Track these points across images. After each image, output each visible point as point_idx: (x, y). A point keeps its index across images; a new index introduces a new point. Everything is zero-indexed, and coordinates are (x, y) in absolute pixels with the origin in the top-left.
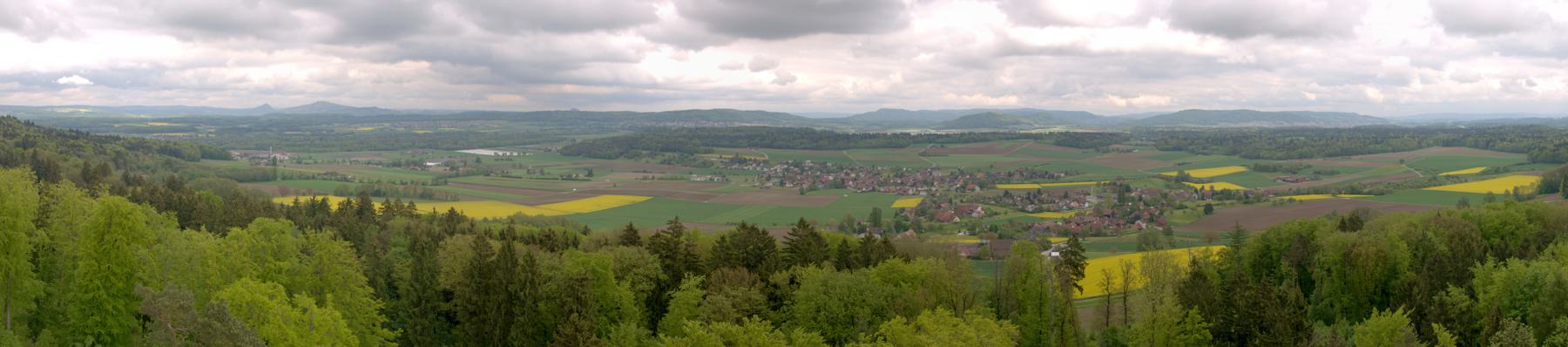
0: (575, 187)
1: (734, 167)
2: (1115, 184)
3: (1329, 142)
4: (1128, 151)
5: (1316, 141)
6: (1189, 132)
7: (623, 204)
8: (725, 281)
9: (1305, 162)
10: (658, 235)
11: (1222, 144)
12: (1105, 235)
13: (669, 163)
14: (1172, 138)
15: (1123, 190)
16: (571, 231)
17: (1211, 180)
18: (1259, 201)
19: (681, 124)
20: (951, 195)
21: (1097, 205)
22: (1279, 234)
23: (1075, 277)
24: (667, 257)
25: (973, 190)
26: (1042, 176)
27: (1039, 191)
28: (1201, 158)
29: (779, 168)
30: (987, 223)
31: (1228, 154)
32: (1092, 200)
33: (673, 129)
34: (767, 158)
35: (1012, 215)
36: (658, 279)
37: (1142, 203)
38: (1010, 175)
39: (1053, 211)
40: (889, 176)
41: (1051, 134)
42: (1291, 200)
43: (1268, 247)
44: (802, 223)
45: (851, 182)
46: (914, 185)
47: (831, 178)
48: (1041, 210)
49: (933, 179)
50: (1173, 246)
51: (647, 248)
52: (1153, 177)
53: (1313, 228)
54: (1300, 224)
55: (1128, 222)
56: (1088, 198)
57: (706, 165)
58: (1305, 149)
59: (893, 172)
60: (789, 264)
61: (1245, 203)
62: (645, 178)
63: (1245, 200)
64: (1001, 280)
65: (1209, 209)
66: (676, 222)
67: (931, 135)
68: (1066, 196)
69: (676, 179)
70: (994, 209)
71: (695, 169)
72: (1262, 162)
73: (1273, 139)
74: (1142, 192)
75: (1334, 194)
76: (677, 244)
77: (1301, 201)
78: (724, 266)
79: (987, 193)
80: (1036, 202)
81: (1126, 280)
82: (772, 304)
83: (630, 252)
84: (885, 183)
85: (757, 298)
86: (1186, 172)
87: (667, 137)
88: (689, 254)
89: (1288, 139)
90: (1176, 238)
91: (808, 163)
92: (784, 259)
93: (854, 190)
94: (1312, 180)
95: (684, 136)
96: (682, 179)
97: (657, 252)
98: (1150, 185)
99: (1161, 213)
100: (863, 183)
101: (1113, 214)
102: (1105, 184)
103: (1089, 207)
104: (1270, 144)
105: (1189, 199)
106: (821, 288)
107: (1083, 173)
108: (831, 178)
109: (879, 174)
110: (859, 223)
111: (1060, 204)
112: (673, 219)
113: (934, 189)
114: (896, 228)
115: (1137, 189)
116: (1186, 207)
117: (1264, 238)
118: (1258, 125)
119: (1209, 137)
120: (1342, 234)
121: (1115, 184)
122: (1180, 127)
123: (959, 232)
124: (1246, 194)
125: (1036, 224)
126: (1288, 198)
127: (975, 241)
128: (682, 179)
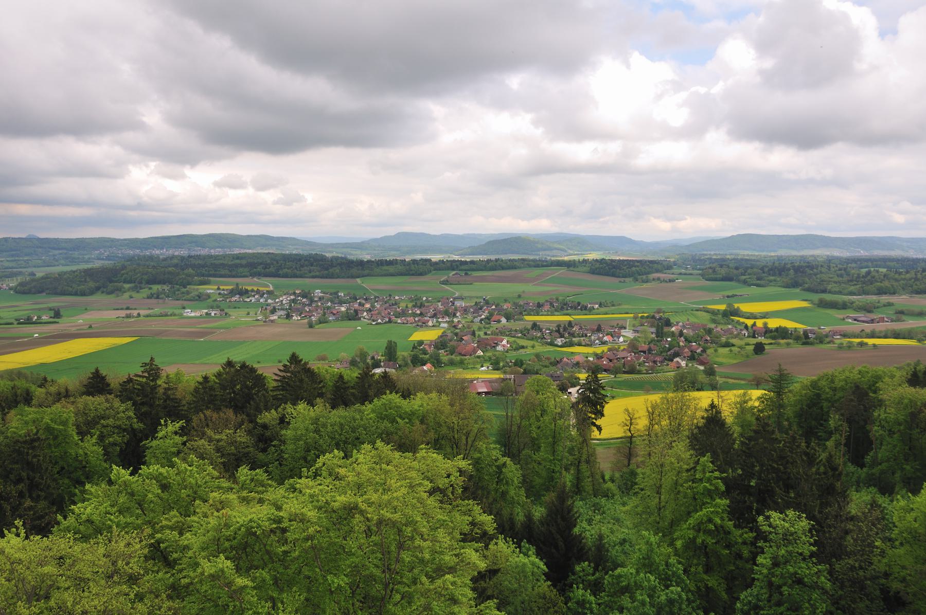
0: (36, 332)
1: (234, 299)
2: (653, 317)
3: (919, 276)
4: (670, 281)
5: (900, 273)
6: (742, 260)
7: (101, 348)
8: (208, 425)
9: (885, 299)
10: (130, 380)
11: (780, 275)
12: (639, 372)
13: (158, 298)
14: (721, 266)
15: (662, 324)
16: (22, 384)
17: (765, 316)
18: (821, 342)
19: (171, 252)
20: (475, 327)
21: (632, 340)
22: (832, 381)
23: (593, 416)
24: (143, 404)
25: (499, 321)
27: (570, 322)
28: (754, 290)
29: (285, 299)
30: (513, 356)
31: (787, 286)
32: (628, 334)
33: (161, 257)
34: (271, 288)
35: (540, 348)
36: (133, 429)
37: (682, 339)
38: (539, 305)
39: (585, 346)
40: (407, 307)
41: (585, 261)
42: (861, 344)
43: (818, 395)
44: (294, 359)
45: (365, 314)
46: (434, 316)
47: (343, 309)
48: (571, 345)
51: (117, 396)
52: (697, 310)
53: (878, 378)
55: (665, 359)
56: (623, 332)
57: (201, 298)
58: (886, 284)
59: (411, 302)
60: (278, 402)
61: (804, 344)
62: (128, 316)
63: (804, 341)
66: (152, 364)
67: (454, 261)
68: (599, 329)
69: (166, 315)
70: (522, 342)
71: (188, 302)
72: (828, 297)
73: (845, 269)
74: (684, 327)
75: (919, 341)
76: (155, 387)
77: (874, 345)
78: (208, 408)
80: (566, 335)
82: (261, 445)
83: (97, 402)
84: (403, 313)
85: (243, 440)
86: (736, 306)
87: (154, 267)
88: (168, 398)
89: (864, 270)
90: (720, 380)
91: (318, 293)
92: (275, 398)
93: (369, 322)
94: (892, 321)
95: (176, 266)
96: (173, 315)
97: (130, 399)
98: (693, 320)
99: (704, 351)
100: (379, 313)
101: (650, 350)
102: (642, 317)
103: (624, 341)
104: (841, 276)
105: (736, 336)
106: (312, 427)
107: (620, 305)
108: (343, 309)
109: (396, 304)
110: (373, 358)
111: (593, 337)
112: (148, 361)
113: (456, 320)
114: (412, 361)
115: (678, 323)
116: (733, 345)
117: (814, 384)
118: (828, 253)
119: (766, 266)
120: (912, 390)
121: (653, 317)
122: (730, 255)
123: (482, 366)
124: (806, 333)
125: (565, 359)
127: (496, 375)
128: (173, 315)
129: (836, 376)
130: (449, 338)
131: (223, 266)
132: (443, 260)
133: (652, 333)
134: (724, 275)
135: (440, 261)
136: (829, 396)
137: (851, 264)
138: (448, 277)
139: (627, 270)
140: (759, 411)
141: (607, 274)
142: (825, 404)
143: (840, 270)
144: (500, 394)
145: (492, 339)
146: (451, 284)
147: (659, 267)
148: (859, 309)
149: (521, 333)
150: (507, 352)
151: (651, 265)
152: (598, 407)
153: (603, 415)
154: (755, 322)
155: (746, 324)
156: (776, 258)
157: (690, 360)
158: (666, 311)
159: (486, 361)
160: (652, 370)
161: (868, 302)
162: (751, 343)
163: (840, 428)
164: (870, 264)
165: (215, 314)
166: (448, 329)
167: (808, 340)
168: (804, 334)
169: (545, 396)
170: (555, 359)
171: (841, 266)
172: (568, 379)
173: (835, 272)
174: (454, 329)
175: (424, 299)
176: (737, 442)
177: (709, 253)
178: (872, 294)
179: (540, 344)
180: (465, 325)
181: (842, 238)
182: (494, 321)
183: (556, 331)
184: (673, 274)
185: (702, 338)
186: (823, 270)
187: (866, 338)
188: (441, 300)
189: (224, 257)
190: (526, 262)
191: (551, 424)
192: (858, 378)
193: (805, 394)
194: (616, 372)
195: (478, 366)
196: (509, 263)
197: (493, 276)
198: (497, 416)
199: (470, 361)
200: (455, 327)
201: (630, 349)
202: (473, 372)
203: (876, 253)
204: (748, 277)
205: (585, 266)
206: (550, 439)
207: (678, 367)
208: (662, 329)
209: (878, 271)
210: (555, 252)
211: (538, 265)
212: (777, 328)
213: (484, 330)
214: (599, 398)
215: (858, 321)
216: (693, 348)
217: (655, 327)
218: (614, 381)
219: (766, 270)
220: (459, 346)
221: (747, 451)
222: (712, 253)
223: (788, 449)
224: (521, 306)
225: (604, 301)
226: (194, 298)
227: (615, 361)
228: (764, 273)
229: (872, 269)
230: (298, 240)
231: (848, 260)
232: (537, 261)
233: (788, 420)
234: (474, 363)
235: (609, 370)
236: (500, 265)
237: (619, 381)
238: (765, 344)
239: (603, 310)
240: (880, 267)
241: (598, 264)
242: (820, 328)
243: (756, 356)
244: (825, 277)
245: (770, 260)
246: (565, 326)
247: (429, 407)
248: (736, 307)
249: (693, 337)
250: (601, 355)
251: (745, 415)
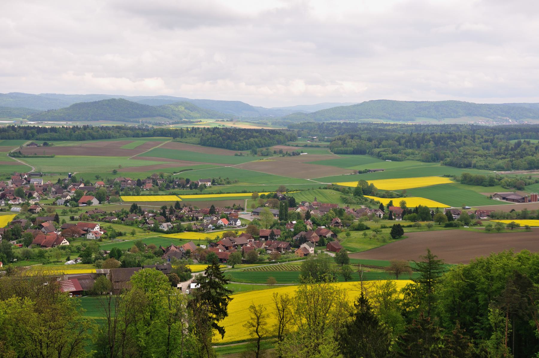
2: (275, 196)
4: (294, 154)
6: (375, 129)
11: (419, 147)
12: (261, 261)
14: (352, 137)
17: (402, 194)
20: (58, 211)
21: (252, 223)
22: (488, 270)
23: (214, 316)
25: (89, 203)
26: (182, 186)
27: (177, 203)
28: (389, 165)
30: (107, 246)
31: (427, 160)
32: (247, 216)
35: (141, 235)
38: (140, 183)
42: (512, 226)
43: (472, 286)
48: (180, 230)
49: (32, 189)
50: (347, 278)
52: (326, 188)
54: (520, 259)
55: (291, 245)
56: (241, 214)
61: (447, 226)
63: (447, 222)
64: (115, 322)
65: (397, 232)
67: (28, 128)
68: (212, 211)
70: (119, 228)
72: (473, 173)
73: (492, 141)
74: (311, 207)
77: (527, 227)
79: (108, 207)
81: (282, 320)
86: (369, 182)
89: (513, 142)
90: (354, 268)
98: (321, 199)
99: (335, 235)
101: (272, 235)
102: (262, 197)
103: (242, 225)
105: (371, 218)
111: (205, 221)
113: (32, 202)
115: (304, 203)
116: (368, 228)
117: (467, 273)
118: (472, 122)
119: (403, 138)
121: (275, 196)
122: (362, 124)
123: (68, 259)
124: (449, 214)
125: (173, 248)
126: (508, 222)
129: (492, 263)
130: (23, 224)
132: (13, 127)
133: (275, 215)
134: (356, 147)
135: (9, 127)
136: (485, 286)
137: (498, 134)
138: (21, 148)
139: (244, 141)
140: (404, 305)
141: (221, 146)
142: (480, 296)
143: (486, 141)
144: (92, 293)
145: (81, 225)
146: (25, 157)
147: (282, 138)
148: (508, 185)
149: (118, 217)
150: (100, 240)
151: (272, 135)
152: (220, 304)
153: (226, 314)
154: (391, 202)
155: (382, 204)
156: (414, 128)
157: (319, 245)
158: (290, 189)
159: (73, 252)
160: (275, 259)
161: (518, 178)
162: (388, 226)
163: (501, 324)
164: (520, 135)
166: (22, 214)
167: (451, 222)
168: (447, 214)
169: (157, 294)
170: (160, 247)
172: (177, 271)
173: (480, 143)
174: (29, 213)
176: (392, 343)
177: (338, 121)
178: (522, 169)
179: (142, 230)
180: (45, 209)
181: (488, 105)
182: (83, 203)
183: (161, 214)
184: (297, 146)
185: (332, 220)
186: (467, 141)
187: (516, 219)
188: (12, 177)
190: (122, 131)
191: (163, 327)
192: (518, 266)
193: (458, 284)
194: (234, 261)
195: (63, 259)
196: (101, 131)
197: (81, 147)
198: (98, 322)
199: (53, 253)
200: (31, 211)
201: (250, 235)
202: (56, 267)
203: (526, 122)
204: (382, 149)
205: (194, 136)
206: (164, 347)
207: (306, 255)
208: (286, 210)
209: (528, 143)
210: (158, 119)
211: (138, 134)
212: (417, 208)
213: (70, 215)
214: (221, 294)
215: (507, 199)
217: (277, 207)
218: (232, 273)
219: (403, 141)
220: (37, 234)
221: (404, 353)
222: (342, 122)
223: (452, 351)
224: (117, 184)
225: (218, 178)
227: (233, 249)
228: (400, 144)
229: (522, 141)
231: (495, 130)
232: (135, 129)
233: (438, 315)
234: (57, 256)
235: (225, 260)
236: (90, 134)
237: (238, 273)
238: (404, 226)
239: (216, 188)
240: (531, 138)
241: (210, 133)
242: (464, 208)
243: (394, 240)
244: (468, 149)
245: (407, 131)
246: (172, 207)
247: (7, 316)
248: (369, 184)
249: (321, 219)
250: (215, 241)
251: (389, 309)
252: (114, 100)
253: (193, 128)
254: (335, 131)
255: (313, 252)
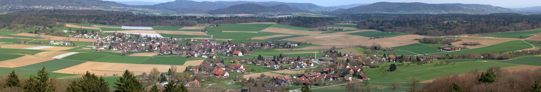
14: (369, 21)
73: (436, 22)
131: (73, 16)
132: (203, 17)
143: (433, 22)
165: (68, 44)
171: (434, 20)
175: (192, 40)
177: (361, 13)
182: (235, 54)
183: (273, 60)
189: (74, 12)
190: (254, 19)
209: (452, 22)
215: (445, 50)
216: (355, 69)
222: (363, 13)
226: (56, 34)
230: (117, 3)
246: (278, 57)
252: (249, 4)
253: (288, 17)
254: (360, 18)
255: (351, 79)
